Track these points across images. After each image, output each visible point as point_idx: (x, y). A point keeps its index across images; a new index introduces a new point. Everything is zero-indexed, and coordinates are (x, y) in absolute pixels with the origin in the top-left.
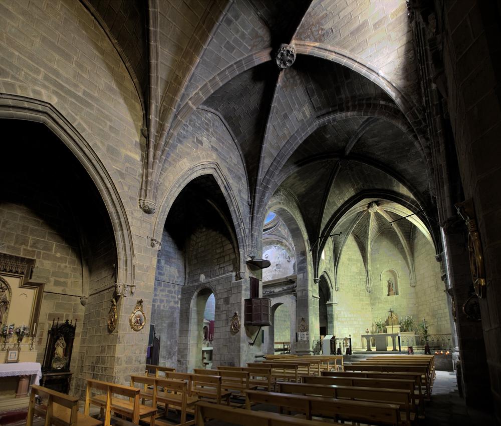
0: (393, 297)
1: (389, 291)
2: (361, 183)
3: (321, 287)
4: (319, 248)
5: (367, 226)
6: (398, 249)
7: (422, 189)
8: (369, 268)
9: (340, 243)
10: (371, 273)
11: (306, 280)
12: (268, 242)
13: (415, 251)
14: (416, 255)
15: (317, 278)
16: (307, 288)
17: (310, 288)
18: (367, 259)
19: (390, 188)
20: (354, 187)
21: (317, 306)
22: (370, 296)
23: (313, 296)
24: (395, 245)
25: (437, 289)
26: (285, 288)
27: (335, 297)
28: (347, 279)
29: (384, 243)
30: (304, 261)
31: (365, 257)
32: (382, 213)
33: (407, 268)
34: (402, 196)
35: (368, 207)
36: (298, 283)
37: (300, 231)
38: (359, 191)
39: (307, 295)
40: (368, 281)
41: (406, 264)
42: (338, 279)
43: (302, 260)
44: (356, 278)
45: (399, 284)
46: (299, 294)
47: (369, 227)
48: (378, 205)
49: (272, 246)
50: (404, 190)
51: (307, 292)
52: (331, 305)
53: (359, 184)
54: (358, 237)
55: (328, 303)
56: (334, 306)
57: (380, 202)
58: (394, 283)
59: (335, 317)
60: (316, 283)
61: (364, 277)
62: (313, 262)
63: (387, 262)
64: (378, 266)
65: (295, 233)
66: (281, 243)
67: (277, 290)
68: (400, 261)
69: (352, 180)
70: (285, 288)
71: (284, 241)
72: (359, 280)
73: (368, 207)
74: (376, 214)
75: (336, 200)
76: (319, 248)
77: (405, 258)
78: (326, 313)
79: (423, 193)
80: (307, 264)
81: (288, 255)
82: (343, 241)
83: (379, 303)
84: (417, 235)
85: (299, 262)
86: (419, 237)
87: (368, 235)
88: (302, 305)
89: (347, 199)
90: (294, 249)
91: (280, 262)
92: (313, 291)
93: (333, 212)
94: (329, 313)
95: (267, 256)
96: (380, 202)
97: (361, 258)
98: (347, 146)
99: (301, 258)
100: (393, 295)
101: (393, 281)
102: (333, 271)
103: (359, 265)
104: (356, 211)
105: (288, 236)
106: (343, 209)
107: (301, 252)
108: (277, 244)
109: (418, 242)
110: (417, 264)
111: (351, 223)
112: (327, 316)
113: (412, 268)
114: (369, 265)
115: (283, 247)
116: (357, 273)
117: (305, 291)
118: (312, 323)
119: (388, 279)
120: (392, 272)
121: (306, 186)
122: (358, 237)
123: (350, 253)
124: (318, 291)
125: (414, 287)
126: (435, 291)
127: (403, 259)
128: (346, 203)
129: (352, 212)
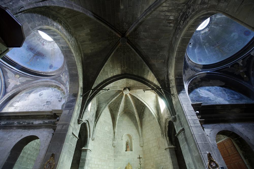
0: (129, 152)
1: (127, 148)
2: (126, 67)
3: (81, 134)
4: (88, 98)
5: (119, 104)
6: (133, 123)
7: (161, 78)
8: (116, 131)
9: (102, 107)
10: (117, 134)
11: (70, 116)
12: (47, 85)
13: (143, 125)
14: (143, 127)
15: (81, 119)
16: (69, 123)
17: (72, 124)
18: (116, 125)
19: (142, 76)
20: (121, 68)
21: (74, 145)
22: (114, 150)
23: (73, 133)
24: (132, 120)
25: (159, 148)
26: (47, 121)
27: (91, 145)
28: (101, 133)
29: (126, 118)
30: (74, 101)
31: (114, 123)
32: (128, 95)
33: (138, 134)
34: (148, 81)
35: (124, 90)
36: (62, 118)
37: (78, 77)
38: (123, 73)
39: (66, 130)
40: (114, 139)
41: (137, 132)
42: (95, 131)
43: (72, 100)
44: (107, 135)
45: (133, 144)
46: (58, 128)
47: (120, 104)
48: (129, 90)
49: (50, 88)
50: (151, 77)
51: (68, 127)
52: (86, 150)
53: (124, 67)
54: (112, 110)
55: (83, 148)
56: (88, 152)
57: (131, 89)
58: (130, 143)
59: (87, 162)
60: (79, 123)
61: (112, 135)
62: (81, 106)
63: (126, 128)
64: (121, 130)
65: (73, 78)
66: (59, 88)
67: (37, 122)
68: (134, 130)
69: (122, 62)
70: (47, 121)
71: (62, 86)
72: (109, 137)
73: (124, 90)
74: (126, 95)
75: (109, 71)
76: (88, 98)
77: (137, 128)
78: (80, 157)
79: (162, 80)
80: (75, 103)
81: (61, 96)
82: (104, 107)
83: (119, 155)
84: (144, 116)
85: (68, 101)
86: (146, 117)
87: (119, 109)
88: (58, 139)
89: (115, 75)
90: (68, 92)
91: (51, 100)
92: (74, 129)
93: (105, 79)
94: (82, 158)
95: (41, 94)
96: (131, 89)
97: (112, 123)
98: (128, 30)
99: (72, 99)
100: (128, 151)
101: (129, 142)
102: (93, 125)
103: (110, 127)
104: (117, 88)
105: (67, 81)
106: (112, 80)
107: (74, 94)
108: (55, 87)
109: (146, 118)
110: (144, 132)
111: (111, 97)
112: (79, 161)
113: (141, 135)
114: (116, 128)
115: (59, 91)
116: (108, 132)
117: (66, 126)
118: (62, 163)
119: (126, 140)
120: (129, 136)
121: (92, 49)
122: (112, 110)
123: (106, 118)
124: (78, 131)
125: (142, 147)
126: (158, 149)
127: (136, 129)
128: (114, 77)
129: (115, 88)
